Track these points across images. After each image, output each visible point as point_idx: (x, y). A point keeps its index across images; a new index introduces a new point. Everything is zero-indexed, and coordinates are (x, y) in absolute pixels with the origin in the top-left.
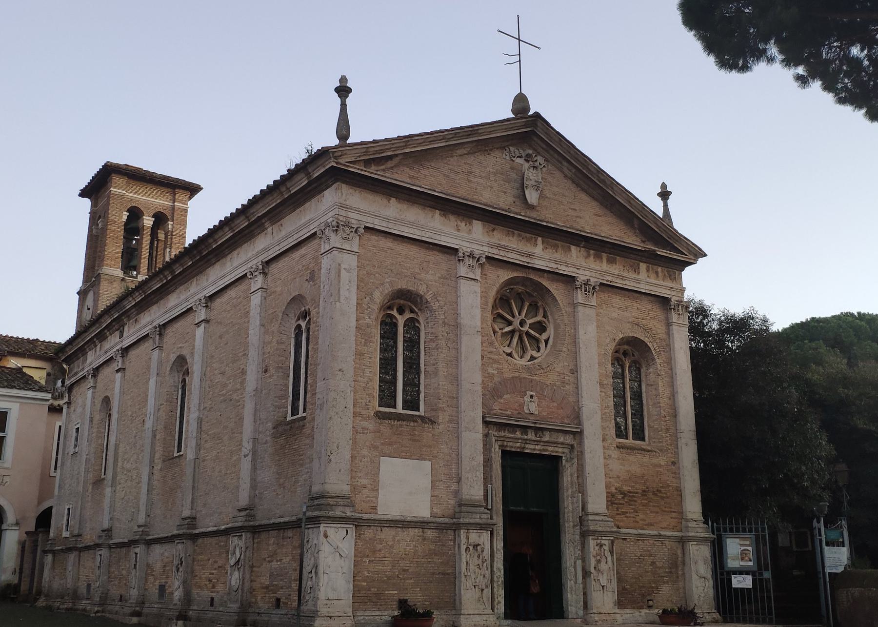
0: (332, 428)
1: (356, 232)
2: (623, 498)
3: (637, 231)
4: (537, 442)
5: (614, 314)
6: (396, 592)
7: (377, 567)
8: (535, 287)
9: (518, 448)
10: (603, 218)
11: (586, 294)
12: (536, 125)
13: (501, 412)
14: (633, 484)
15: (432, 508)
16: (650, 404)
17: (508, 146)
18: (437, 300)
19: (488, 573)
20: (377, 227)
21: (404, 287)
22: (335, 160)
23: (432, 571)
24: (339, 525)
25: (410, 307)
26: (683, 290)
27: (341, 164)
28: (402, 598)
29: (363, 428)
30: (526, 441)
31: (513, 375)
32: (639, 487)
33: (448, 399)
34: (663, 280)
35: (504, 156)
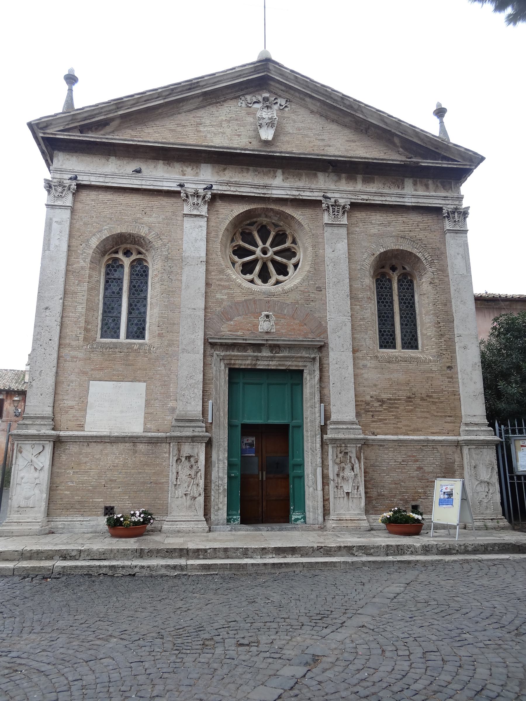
0: (35, 358)
1: (69, 189)
2: (381, 405)
3: (401, 149)
4: (272, 358)
5: (374, 231)
6: (102, 500)
7: (81, 478)
8: (278, 216)
9: (248, 365)
10: (357, 143)
11: (335, 214)
12: (269, 69)
13: (231, 333)
14: (395, 392)
15: (145, 424)
16: (424, 312)
17: (243, 95)
18: (161, 239)
19: (202, 482)
20: (93, 183)
21: (124, 231)
22: (42, 131)
23: (143, 480)
24: (34, 442)
25: (137, 249)
26: (460, 198)
27: (48, 134)
28: (108, 505)
29: (73, 357)
30: (257, 359)
31: (245, 298)
32: (403, 394)
33: (167, 326)
34: (435, 192)
35: (239, 105)
